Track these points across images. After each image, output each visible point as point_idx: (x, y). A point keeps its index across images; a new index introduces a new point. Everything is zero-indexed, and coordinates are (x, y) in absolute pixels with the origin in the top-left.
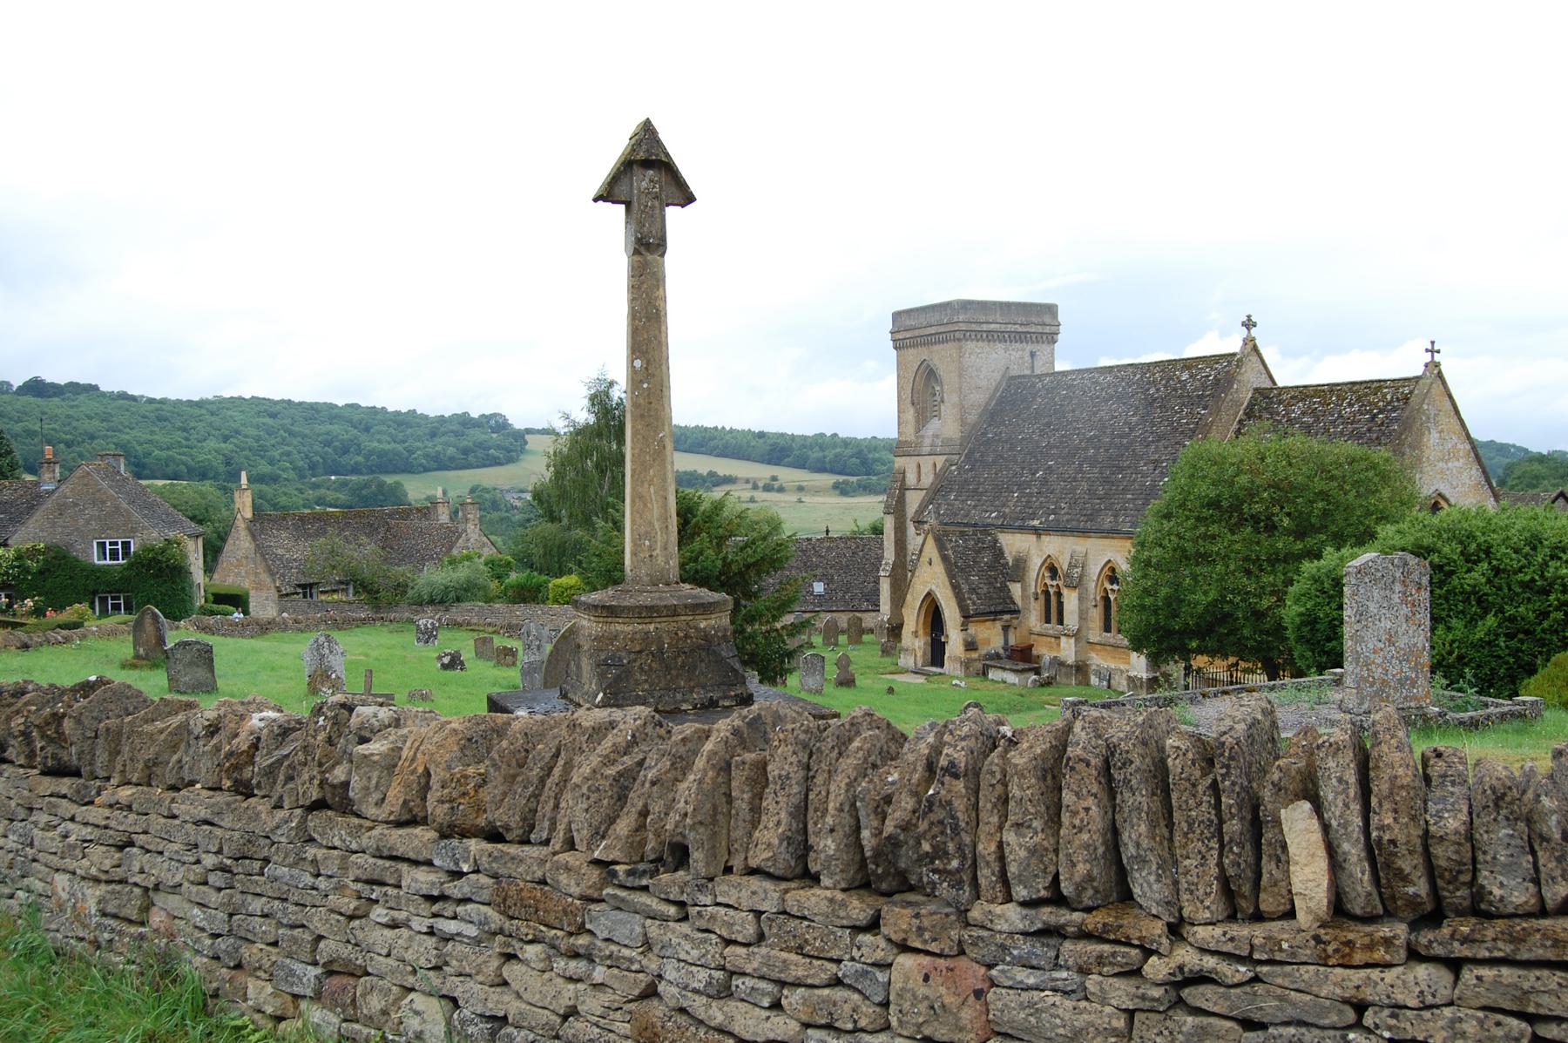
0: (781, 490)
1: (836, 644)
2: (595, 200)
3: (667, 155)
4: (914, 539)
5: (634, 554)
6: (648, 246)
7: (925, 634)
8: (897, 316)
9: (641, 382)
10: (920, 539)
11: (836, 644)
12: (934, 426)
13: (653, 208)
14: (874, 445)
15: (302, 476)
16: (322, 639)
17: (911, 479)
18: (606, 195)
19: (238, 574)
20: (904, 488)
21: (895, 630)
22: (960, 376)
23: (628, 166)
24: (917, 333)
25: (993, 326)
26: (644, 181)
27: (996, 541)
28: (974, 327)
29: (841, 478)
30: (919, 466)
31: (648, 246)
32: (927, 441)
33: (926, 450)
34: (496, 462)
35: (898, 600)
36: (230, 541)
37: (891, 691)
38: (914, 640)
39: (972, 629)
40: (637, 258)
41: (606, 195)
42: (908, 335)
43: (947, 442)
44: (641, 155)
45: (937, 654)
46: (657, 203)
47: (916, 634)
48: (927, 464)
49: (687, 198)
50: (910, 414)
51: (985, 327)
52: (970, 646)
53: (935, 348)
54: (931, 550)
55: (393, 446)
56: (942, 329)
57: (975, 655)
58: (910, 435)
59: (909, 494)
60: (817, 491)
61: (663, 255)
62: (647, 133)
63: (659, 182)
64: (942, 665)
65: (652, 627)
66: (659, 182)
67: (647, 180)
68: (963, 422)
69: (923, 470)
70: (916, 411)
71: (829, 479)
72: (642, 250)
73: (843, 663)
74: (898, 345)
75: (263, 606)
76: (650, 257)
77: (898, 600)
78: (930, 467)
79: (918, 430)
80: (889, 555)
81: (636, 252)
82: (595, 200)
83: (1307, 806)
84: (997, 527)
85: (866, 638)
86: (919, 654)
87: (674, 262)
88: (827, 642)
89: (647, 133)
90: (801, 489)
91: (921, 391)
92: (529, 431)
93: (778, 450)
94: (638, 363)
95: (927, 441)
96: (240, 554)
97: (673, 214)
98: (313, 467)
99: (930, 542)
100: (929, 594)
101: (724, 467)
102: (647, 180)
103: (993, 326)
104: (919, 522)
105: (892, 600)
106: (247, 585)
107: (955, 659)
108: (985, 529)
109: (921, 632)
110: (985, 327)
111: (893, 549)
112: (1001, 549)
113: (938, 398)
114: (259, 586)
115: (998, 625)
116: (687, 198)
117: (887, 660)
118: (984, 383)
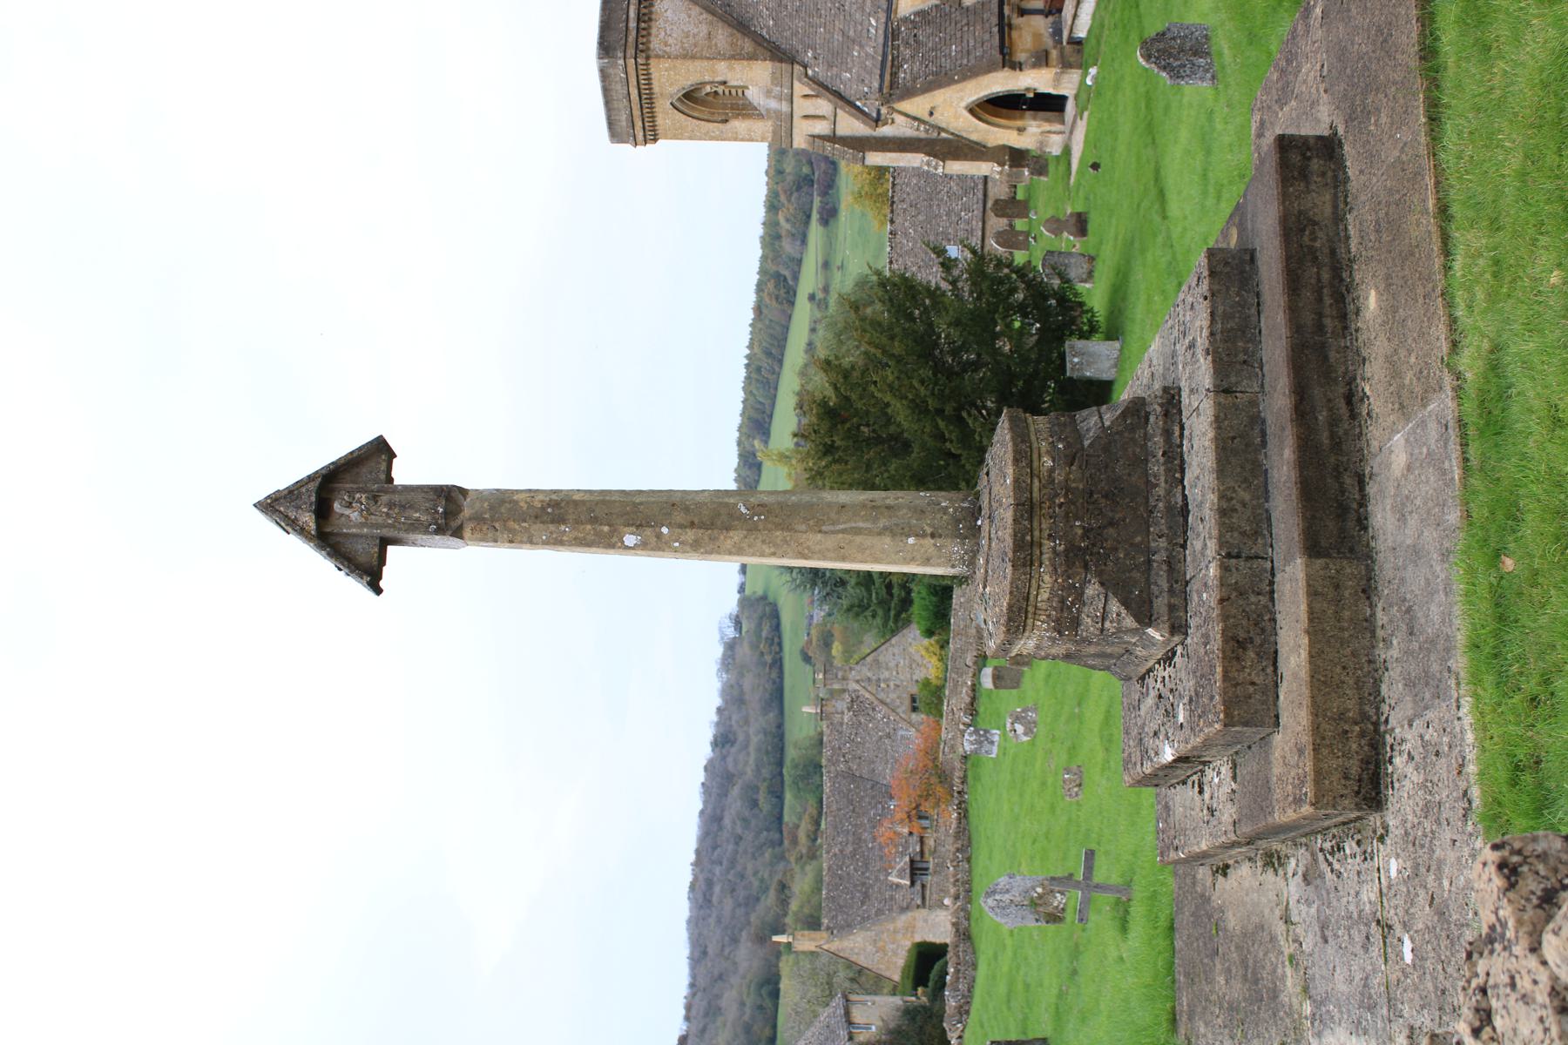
0: (826, 289)
1: (1027, 234)
2: (378, 591)
3: (310, 478)
4: (899, 127)
5: (927, 561)
6: (447, 513)
7: (1022, 118)
8: (616, 135)
9: (659, 536)
10: (899, 119)
11: (1027, 234)
12: (754, 95)
13: (391, 505)
14: (776, 172)
15: (782, 857)
16: (990, 902)
17: (822, 128)
18: (372, 576)
19: (895, 953)
20: (833, 138)
21: (1017, 157)
22: (693, 57)
23: (328, 540)
24: (637, 113)
25: (632, 14)
26: (349, 514)
27: (905, 20)
28: (632, 38)
29: (815, 216)
30: (806, 117)
31: (447, 513)
32: (773, 104)
33: (785, 107)
34: (777, 628)
35: (975, 151)
36: (854, 958)
37: (1095, 166)
38: (1031, 134)
39: (1021, 56)
40: (467, 533)
41: (372, 576)
42: (639, 124)
43: (776, 80)
44: (308, 519)
45: (1049, 105)
46: (385, 498)
47: (1021, 130)
48: (802, 107)
49: (380, 451)
50: (738, 125)
51: (632, 24)
52: (1042, 59)
53: (656, 88)
54: (917, 105)
55: (752, 749)
56: (633, 81)
57: (1054, 54)
58: (765, 127)
59: (841, 132)
60: (830, 244)
61: (463, 492)
62: (273, 506)
63: (351, 493)
64: (1063, 98)
65: (1048, 544)
66: (351, 493)
67: (351, 510)
68: (752, 57)
69: (811, 112)
70: (736, 116)
71: (815, 231)
72: (454, 524)
73: (1056, 225)
74: (651, 135)
75: (937, 927)
76: (467, 512)
77: (975, 151)
78: (808, 102)
79: (761, 116)
80: (915, 160)
81: (458, 533)
82: (378, 591)
83: (390, 549)
84: (888, 18)
85: (1020, 196)
86: (1047, 127)
87: (478, 474)
88: (1025, 246)
89: (273, 506)
90: (826, 265)
91: (710, 107)
92: (742, 589)
93: (777, 287)
94: (630, 540)
95: (773, 104)
96: (870, 948)
97: (405, 473)
98: (773, 844)
99: (906, 106)
100: (971, 111)
101: (795, 355)
102: (351, 510)
103: (632, 14)
104: (877, 121)
105: (973, 159)
106: (908, 944)
107: (1057, 81)
108: (891, 34)
109: (1019, 123)
110: (632, 24)
111: (909, 156)
112: (917, 14)
113: (720, 89)
114: (910, 928)
115: (1017, 21)
116: (380, 451)
117: (1051, 168)
118: (704, 29)
